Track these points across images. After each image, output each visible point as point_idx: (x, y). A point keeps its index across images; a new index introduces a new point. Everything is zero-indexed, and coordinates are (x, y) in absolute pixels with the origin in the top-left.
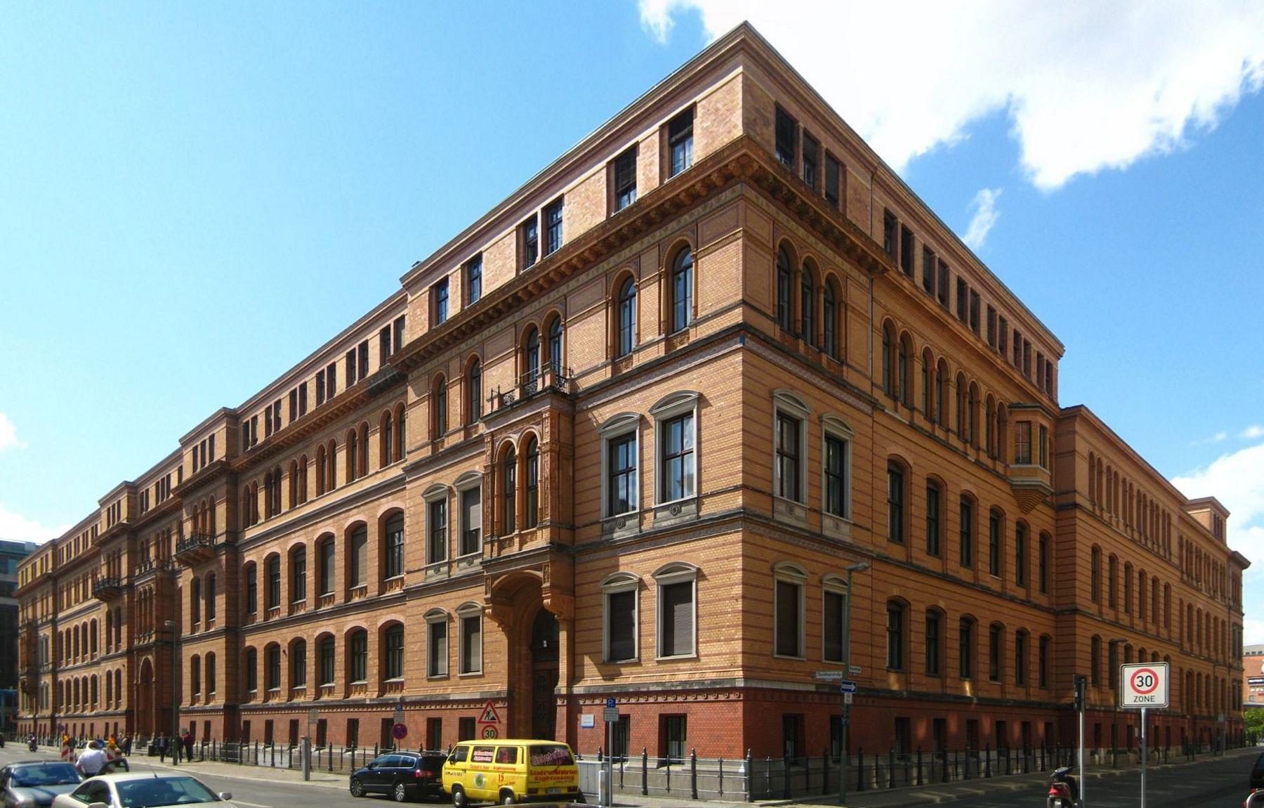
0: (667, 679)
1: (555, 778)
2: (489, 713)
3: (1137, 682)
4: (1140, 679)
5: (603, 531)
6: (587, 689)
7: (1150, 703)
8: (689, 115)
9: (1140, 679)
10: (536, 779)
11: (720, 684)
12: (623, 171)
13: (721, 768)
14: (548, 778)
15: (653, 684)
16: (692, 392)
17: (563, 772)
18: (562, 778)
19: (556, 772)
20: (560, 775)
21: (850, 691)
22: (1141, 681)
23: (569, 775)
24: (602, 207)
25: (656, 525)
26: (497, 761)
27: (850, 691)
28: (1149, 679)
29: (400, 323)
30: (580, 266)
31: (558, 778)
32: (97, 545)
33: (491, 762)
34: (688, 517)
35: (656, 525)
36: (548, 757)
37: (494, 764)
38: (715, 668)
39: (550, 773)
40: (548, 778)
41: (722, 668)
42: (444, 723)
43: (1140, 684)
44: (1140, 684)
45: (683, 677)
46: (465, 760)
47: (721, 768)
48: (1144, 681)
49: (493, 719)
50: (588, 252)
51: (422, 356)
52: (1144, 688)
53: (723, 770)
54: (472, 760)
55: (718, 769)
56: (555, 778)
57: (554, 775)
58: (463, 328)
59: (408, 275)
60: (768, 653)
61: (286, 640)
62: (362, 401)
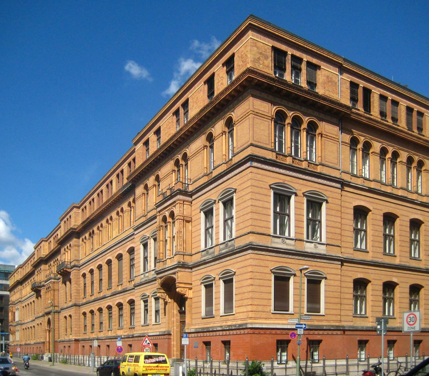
0: (224, 324)
1: (157, 369)
2: (146, 341)
3: (409, 320)
4: (410, 318)
5: (201, 256)
6: (196, 329)
7: (414, 330)
8: (187, 100)
9: (410, 318)
10: (146, 369)
11: (241, 326)
12: (210, 82)
13: (237, 365)
14: (152, 369)
15: (218, 327)
16: (233, 188)
17: (162, 367)
18: (160, 369)
19: (157, 366)
20: (160, 368)
21: (302, 328)
22: (410, 319)
23: (164, 368)
24: (237, 65)
25: (220, 252)
26: (134, 362)
27: (302, 328)
28: (413, 318)
29: (134, 160)
30: (193, 131)
31: (158, 369)
32: (59, 244)
33: (132, 362)
34: (231, 248)
35: (220, 252)
36: (154, 360)
37: (133, 363)
38: (241, 319)
39: (154, 367)
40: (152, 369)
41: (243, 319)
42: (211, 343)
43: (410, 321)
44: (410, 321)
45: (229, 323)
46: (125, 362)
47: (237, 365)
48: (411, 319)
49: (149, 343)
50: (228, 96)
51: (186, 134)
52: (411, 323)
53: (239, 366)
54: (128, 362)
55: (236, 366)
56: (157, 369)
57: (157, 368)
58: (152, 163)
59: (35, 246)
60: (268, 311)
61: (96, 309)
62: (121, 198)
